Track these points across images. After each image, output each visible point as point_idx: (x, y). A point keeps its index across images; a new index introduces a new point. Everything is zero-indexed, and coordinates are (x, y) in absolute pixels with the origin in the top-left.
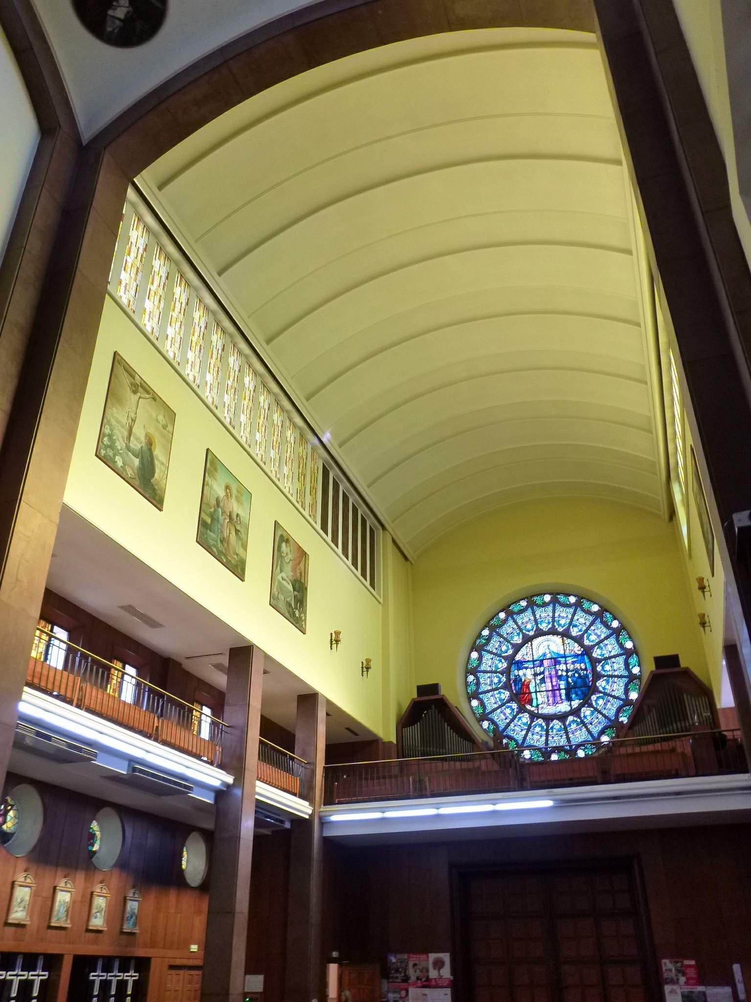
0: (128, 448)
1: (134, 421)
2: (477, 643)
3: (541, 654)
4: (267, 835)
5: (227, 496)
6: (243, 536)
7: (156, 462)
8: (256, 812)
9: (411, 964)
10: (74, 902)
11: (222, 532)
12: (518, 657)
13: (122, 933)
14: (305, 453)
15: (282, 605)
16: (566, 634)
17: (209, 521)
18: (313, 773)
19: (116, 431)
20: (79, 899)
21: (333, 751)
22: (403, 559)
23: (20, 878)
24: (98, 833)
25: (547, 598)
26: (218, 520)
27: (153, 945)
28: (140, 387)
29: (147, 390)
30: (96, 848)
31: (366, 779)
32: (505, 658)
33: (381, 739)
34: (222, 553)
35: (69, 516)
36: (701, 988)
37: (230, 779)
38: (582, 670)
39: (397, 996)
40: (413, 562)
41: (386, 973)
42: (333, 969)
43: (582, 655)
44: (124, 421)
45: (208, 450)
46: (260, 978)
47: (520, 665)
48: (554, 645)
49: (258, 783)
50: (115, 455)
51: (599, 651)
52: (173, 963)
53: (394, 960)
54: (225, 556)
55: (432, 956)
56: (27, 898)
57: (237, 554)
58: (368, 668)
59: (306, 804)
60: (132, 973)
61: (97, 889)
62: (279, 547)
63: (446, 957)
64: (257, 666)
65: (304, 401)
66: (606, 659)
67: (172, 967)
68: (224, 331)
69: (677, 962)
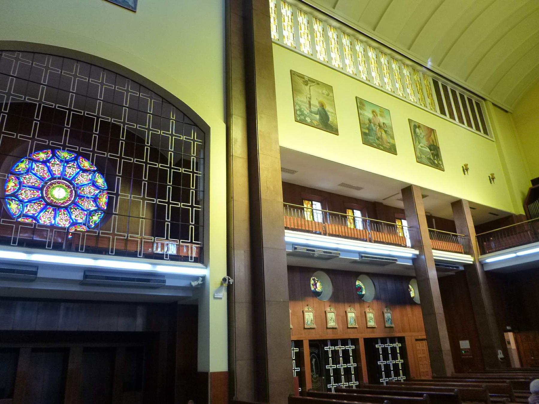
0: (311, 112)
1: (310, 98)
5: (374, 116)
6: (390, 132)
7: (329, 113)
8: (436, 265)
10: (357, 317)
11: (376, 134)
13: (385, 327)
14: (418, 78)
15: (425, 160)
17: (367, 131)
18: (469, 240)
19: (302, 107)
20: (359, 315)
21: (478, 228)
22: (505, 113)
23: (328, 309)
24: (363, 286)
26: (372, 129)
27: (404, 331)
28: (309, 81)
29: (312, 81)
30: (364, 293)
31: (501, 237)
33: (514, 214)
34: (380, 145)
35: (285, 153)
37: (417, 252)
40: (510, 111)
42: (510, 336)
44: (305, 100)
45: (356, 97)
46: (467, 342)
49: (433, 251)
50: (305, 118)
52: (417, 338)
54: (382, 145)
56: (334, 317)
57: (389, 143)
58: (493, 179)
59: (470, 256)
60: (397, 343)
61: (367, 310)
62: (415, 132)
64: (417, 195)
65: (408, 51)
67: (417, 340)
68: (349, 35)
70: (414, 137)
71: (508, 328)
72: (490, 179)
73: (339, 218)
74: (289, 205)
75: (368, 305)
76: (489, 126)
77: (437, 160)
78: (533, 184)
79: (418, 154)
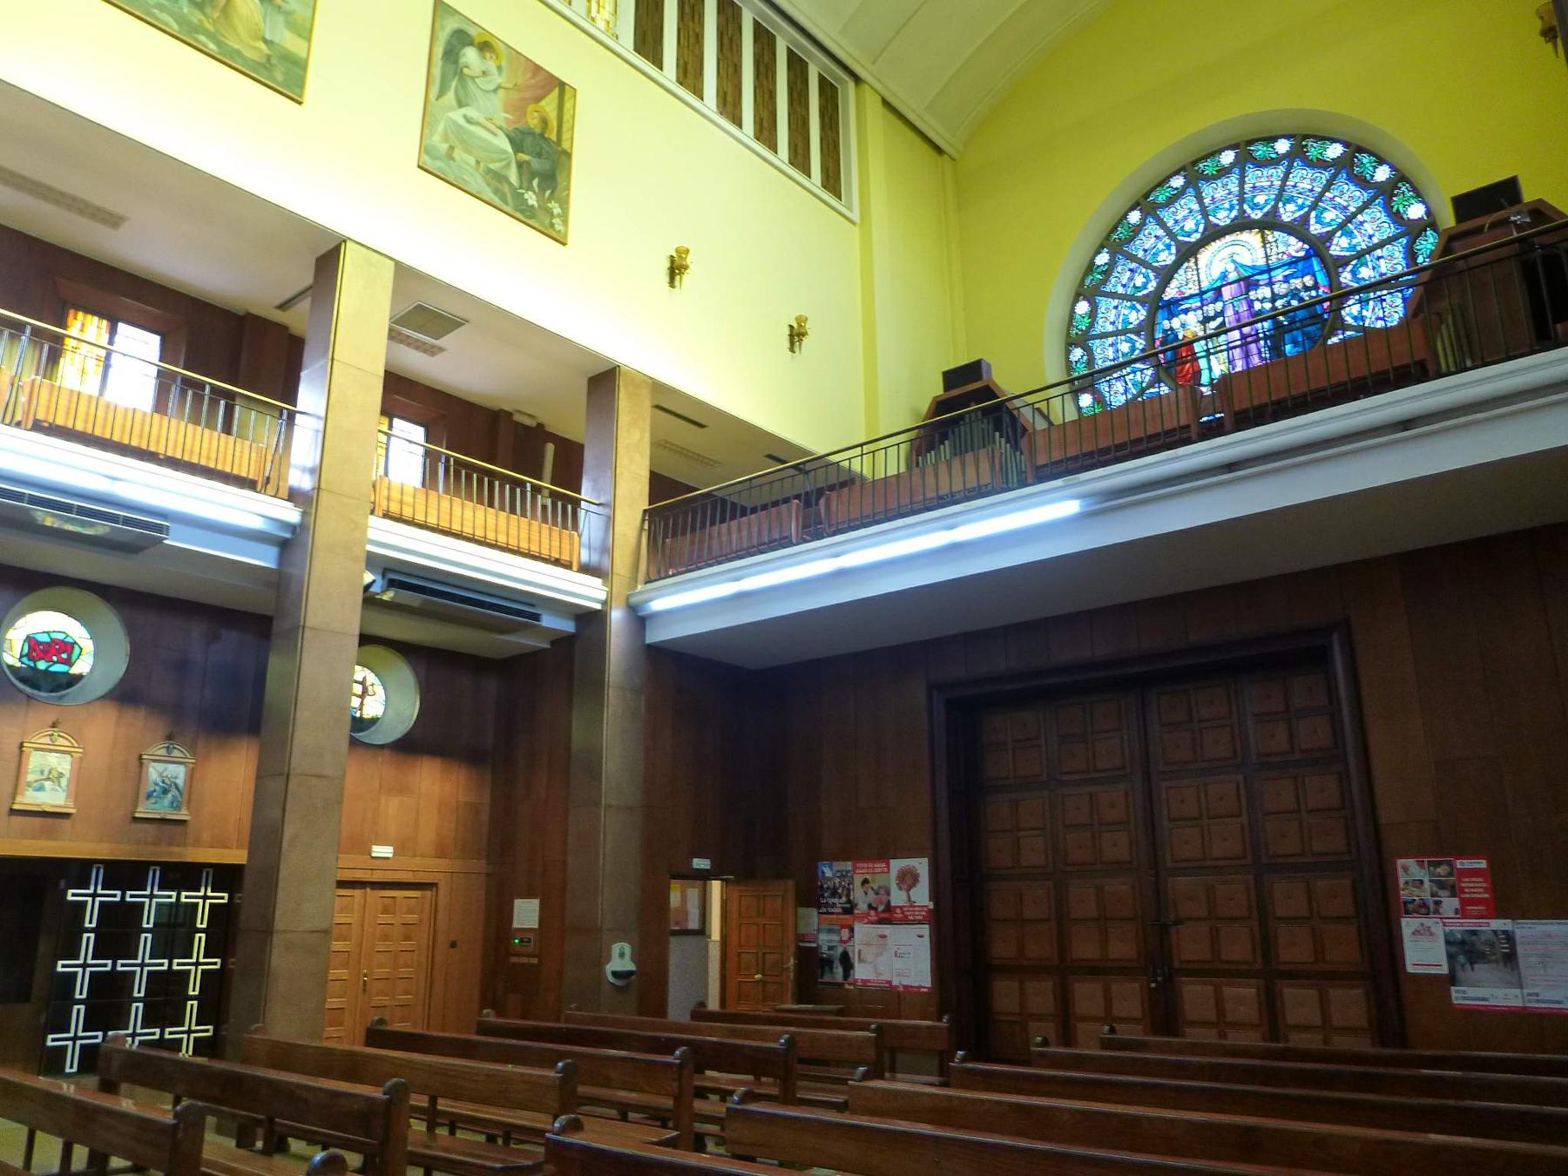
2: (1087, 282)
3: (1216, 275)
4: (543, 650)
9: (858, 880)
12: (1170, 293)
16: (1270, 223)
22: (931, 152)
25: (1228, 157)
32: (1142, 301)
36: (1497, 924)
38: (1307, 289)
39: (836, 938)
41: (811, 895)
43: (1307, 258)
47: (1172, 308)
48: (1248, 249)
49: (375, 522)
51: (1344, 242)
53: (828, 873)
55: (897, 865)
59: (598, 582)
63: (922, 866)
66: (1360, 255)
67: (342, 884)
69: (1439, 864)
70: (437, 72)
71: (701, 863)
72: (791, 336)
73: (198, 399)
74: (213, 387)
75: (51, 718)
76: (849, 173)
77: (540, 195)
78: (947, 388)
79: (436, 138)
